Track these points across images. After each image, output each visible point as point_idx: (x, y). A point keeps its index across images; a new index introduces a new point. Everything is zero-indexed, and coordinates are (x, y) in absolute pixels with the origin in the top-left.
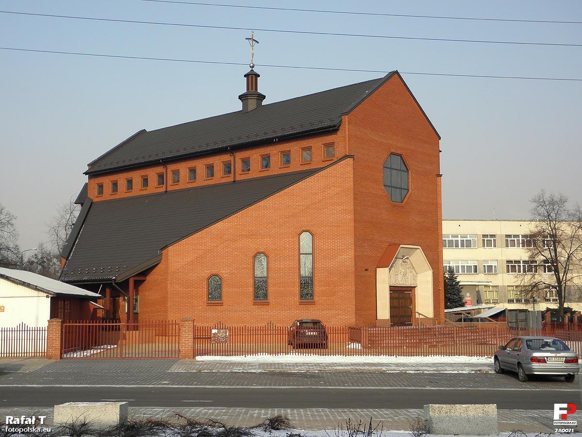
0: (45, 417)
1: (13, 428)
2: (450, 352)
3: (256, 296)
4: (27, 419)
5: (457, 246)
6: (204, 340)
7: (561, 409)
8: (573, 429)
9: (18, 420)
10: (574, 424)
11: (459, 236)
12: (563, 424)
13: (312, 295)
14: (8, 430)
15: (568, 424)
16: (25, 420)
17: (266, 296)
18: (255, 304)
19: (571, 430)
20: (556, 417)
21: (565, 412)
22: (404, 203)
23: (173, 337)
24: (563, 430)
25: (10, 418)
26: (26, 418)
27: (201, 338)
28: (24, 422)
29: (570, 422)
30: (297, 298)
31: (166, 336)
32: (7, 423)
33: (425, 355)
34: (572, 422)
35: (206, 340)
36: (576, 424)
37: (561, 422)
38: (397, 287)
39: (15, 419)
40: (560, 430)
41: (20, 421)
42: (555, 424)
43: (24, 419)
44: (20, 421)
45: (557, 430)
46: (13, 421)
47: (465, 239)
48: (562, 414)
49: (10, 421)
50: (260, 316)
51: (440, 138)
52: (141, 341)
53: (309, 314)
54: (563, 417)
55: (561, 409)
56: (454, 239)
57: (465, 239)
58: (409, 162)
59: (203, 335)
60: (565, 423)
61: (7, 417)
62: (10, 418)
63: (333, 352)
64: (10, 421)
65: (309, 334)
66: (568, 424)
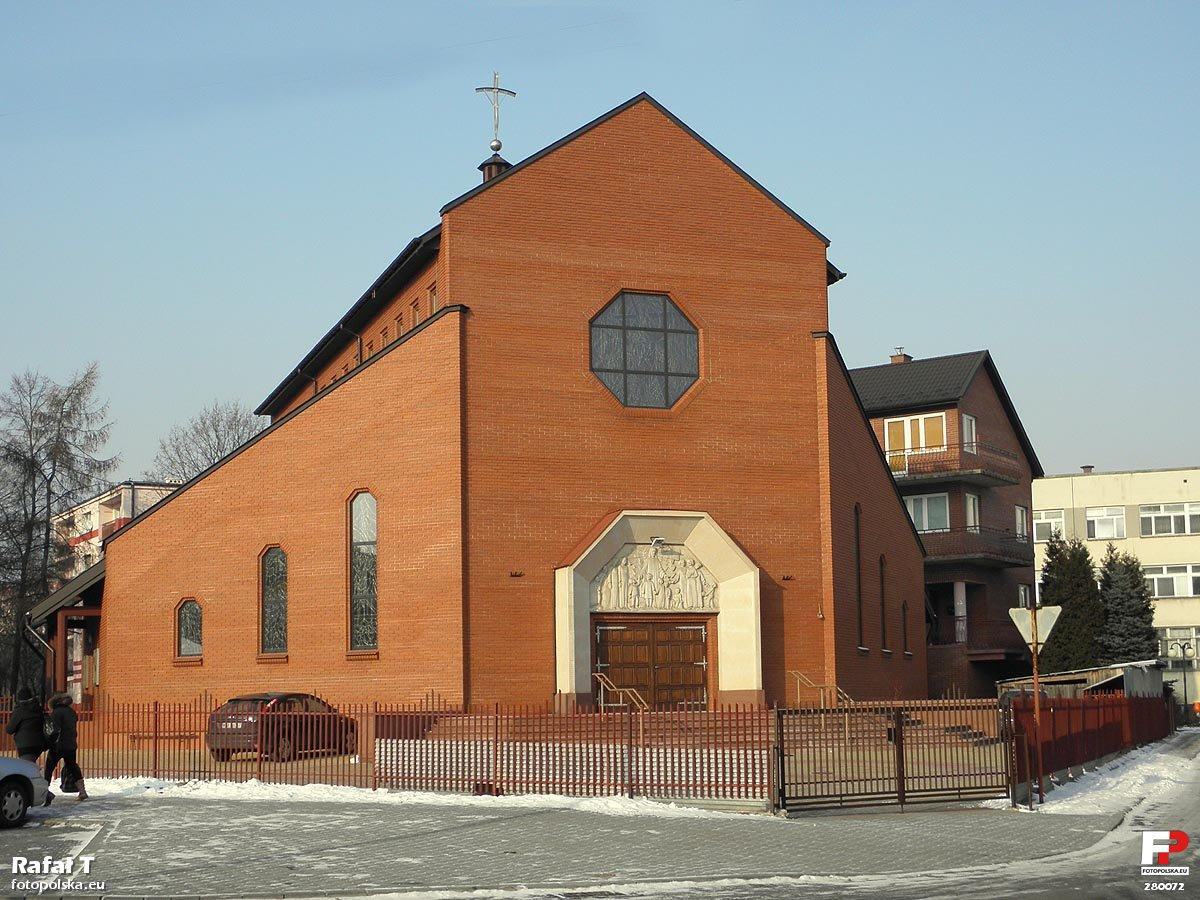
0: (93, 859)
1: (28, 882)
2: (197, 769)
3: (264, 646)
4: (55, 863)
5: (1181, 528)
6: (167, 741)
7: (1157, 842)
8: (1182, 885)
9: (37, 864)
10: (1183, 874)
11: (1162, 507)
12: (1160, 873)
13: (375, 637)
14: (16, 885)
15: (1172, 874)
16: (51, 866)
17: (283, 644)
18: (260, 660)
19: (1179, 886)
20: (1147, 858)
21: (1165, 849)
22: (673, 410)
23: (742, 711)
24: (1162, 887)
25: (20, 862)
26: (53, 860)
27: (177, 738)
28: (50, 870)
29: (1175, 868)
30: (342, 647)
31: (113, 733)
32: (15, 871)
33: (239, 779)
34: (1179, 869)
35: (167, 741)
36: (1187, 874)
37: (1158, 868)
38: (663, 614)
39: (31, 863)
40: (1154, 885)
41: (42, 867)
42: (1145, 874)
43: (50, 862)
44: (42, 867)
45: (1148, 885)
46: (26, 867)
47: (1153, 515)
48: (1159, 853)
49: (22, 866)
50: (182, 690)
51: (827, 243)
52: (86, 746)
53: (278, 682)
54: (1161, 859)
55: (1157, 842)
56: (1172, 514)
57: (1153, 515)
58: (693, 309)
59: (174, 731)
60: (1165, 870)
61: (15, 859)
62: (20, 862)
63: (143, 770)
64: (22, 866)
65: (234, 727)
66: (1172, 874)
